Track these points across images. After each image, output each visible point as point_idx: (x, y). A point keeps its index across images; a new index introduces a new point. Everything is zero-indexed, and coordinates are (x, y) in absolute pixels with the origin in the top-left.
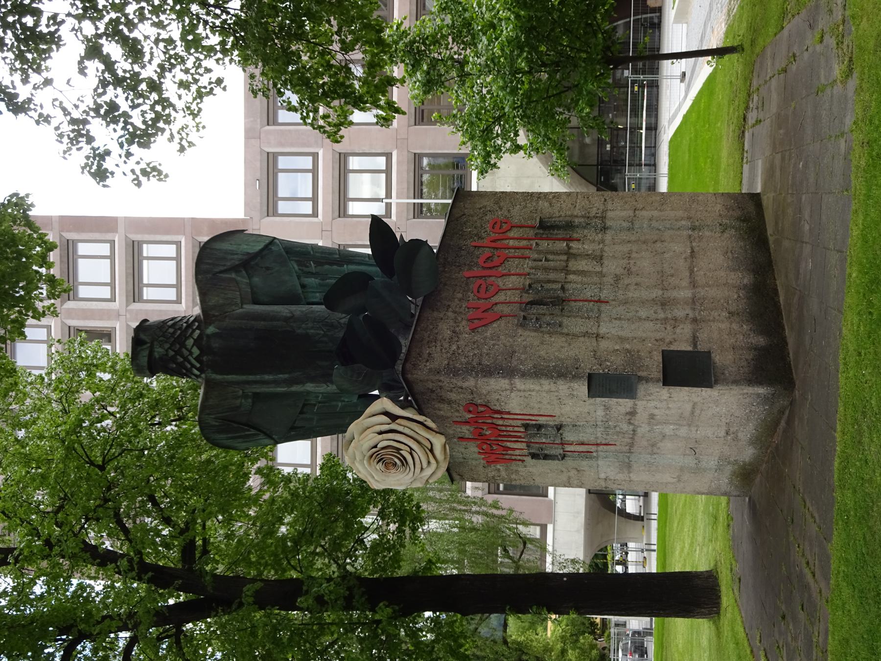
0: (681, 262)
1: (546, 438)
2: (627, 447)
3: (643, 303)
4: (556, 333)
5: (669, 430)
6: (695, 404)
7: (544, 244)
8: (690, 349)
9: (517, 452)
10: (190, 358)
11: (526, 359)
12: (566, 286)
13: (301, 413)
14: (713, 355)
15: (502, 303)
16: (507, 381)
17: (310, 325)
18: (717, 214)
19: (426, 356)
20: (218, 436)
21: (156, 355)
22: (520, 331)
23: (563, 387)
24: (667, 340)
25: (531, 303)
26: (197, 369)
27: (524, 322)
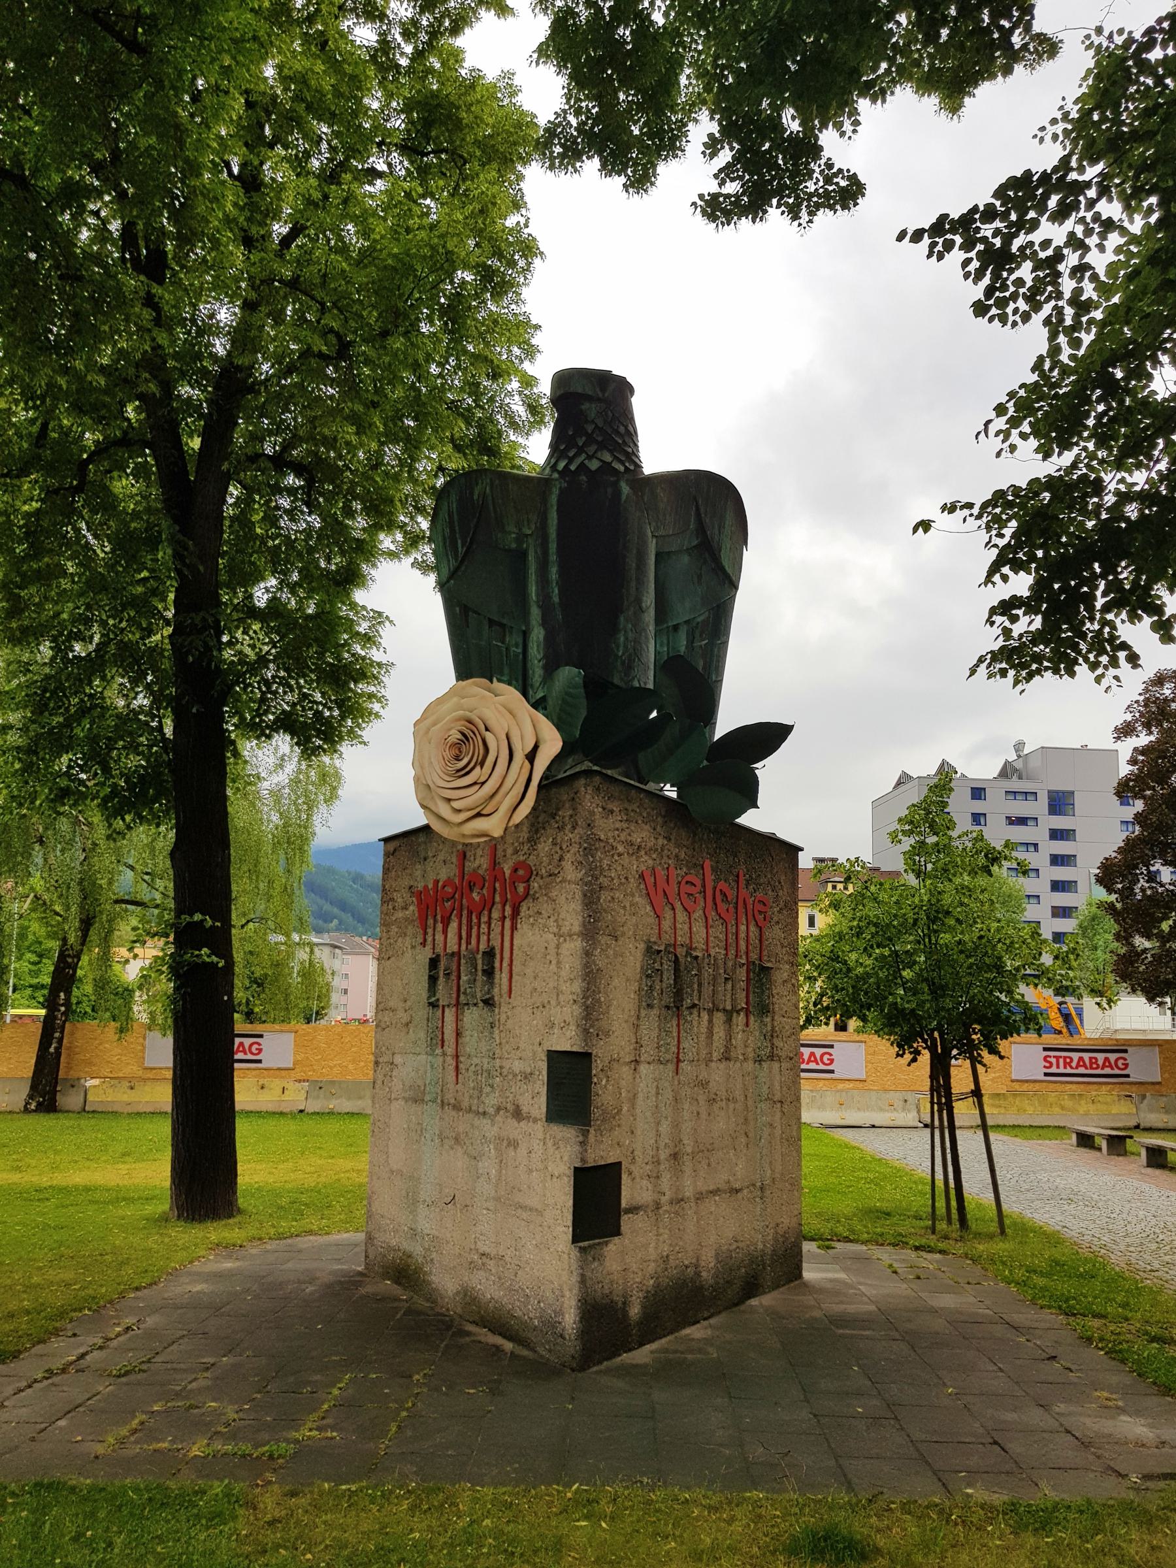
0: (724, 1176)
1: (469, 982)
2: (452, 1101)
3: (676, 1125)
4: (640, 1001)
5: (488, 1165)
6: (540, 1213)
7: (742, 973)
8: (624, 1204)
9: (439, 937)
10: (583, 456)
11: (608, 957)
12: (695, 1011)
13: (491, 622)
14: (616, 1239)
15: (761, 935)
16: (577, 928)
17: (630, 635)
18: (779, 1221)
19: (610, 806)
20: (454, 498)
21: (586, 406)
22: (642, 946)
23: (569, 1012)
24: (633, 1168)
25: (677, 961)
26: (566, 466)
27: (651, 951)
